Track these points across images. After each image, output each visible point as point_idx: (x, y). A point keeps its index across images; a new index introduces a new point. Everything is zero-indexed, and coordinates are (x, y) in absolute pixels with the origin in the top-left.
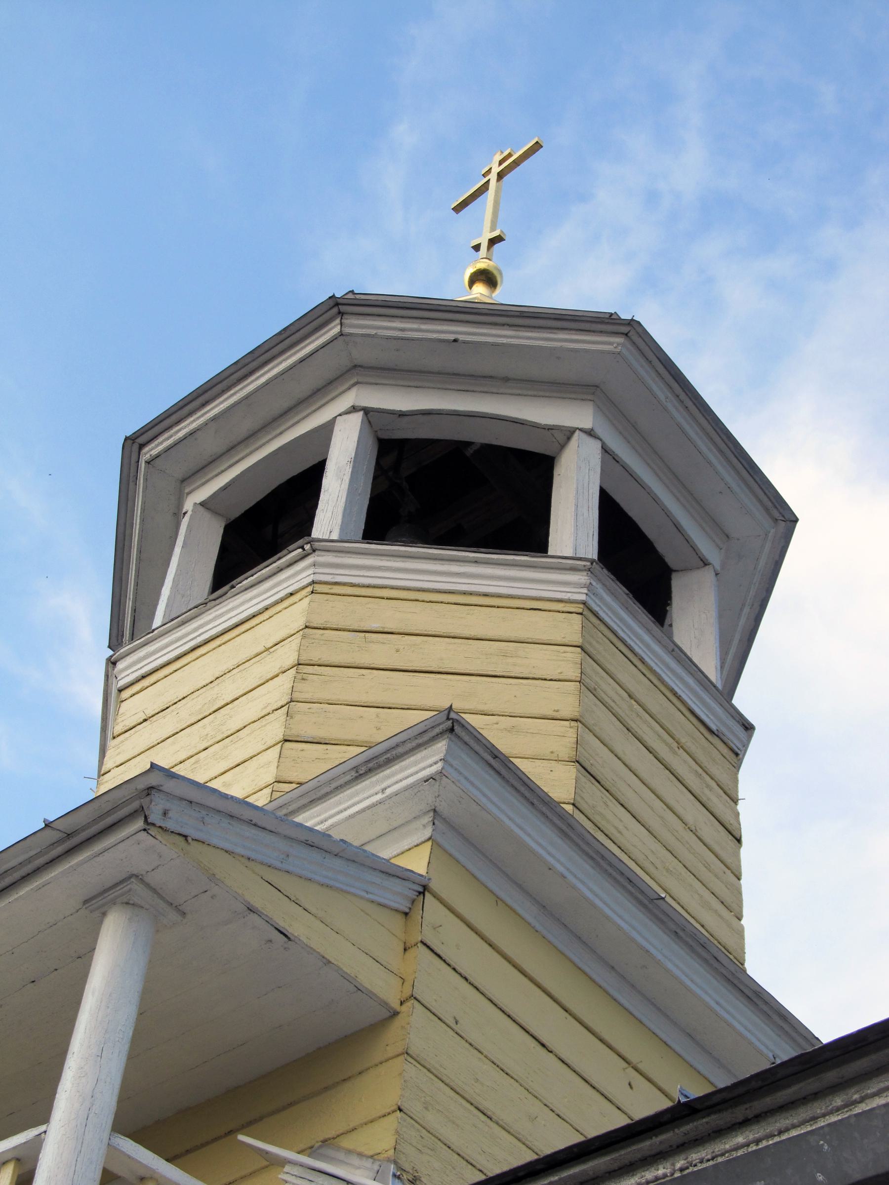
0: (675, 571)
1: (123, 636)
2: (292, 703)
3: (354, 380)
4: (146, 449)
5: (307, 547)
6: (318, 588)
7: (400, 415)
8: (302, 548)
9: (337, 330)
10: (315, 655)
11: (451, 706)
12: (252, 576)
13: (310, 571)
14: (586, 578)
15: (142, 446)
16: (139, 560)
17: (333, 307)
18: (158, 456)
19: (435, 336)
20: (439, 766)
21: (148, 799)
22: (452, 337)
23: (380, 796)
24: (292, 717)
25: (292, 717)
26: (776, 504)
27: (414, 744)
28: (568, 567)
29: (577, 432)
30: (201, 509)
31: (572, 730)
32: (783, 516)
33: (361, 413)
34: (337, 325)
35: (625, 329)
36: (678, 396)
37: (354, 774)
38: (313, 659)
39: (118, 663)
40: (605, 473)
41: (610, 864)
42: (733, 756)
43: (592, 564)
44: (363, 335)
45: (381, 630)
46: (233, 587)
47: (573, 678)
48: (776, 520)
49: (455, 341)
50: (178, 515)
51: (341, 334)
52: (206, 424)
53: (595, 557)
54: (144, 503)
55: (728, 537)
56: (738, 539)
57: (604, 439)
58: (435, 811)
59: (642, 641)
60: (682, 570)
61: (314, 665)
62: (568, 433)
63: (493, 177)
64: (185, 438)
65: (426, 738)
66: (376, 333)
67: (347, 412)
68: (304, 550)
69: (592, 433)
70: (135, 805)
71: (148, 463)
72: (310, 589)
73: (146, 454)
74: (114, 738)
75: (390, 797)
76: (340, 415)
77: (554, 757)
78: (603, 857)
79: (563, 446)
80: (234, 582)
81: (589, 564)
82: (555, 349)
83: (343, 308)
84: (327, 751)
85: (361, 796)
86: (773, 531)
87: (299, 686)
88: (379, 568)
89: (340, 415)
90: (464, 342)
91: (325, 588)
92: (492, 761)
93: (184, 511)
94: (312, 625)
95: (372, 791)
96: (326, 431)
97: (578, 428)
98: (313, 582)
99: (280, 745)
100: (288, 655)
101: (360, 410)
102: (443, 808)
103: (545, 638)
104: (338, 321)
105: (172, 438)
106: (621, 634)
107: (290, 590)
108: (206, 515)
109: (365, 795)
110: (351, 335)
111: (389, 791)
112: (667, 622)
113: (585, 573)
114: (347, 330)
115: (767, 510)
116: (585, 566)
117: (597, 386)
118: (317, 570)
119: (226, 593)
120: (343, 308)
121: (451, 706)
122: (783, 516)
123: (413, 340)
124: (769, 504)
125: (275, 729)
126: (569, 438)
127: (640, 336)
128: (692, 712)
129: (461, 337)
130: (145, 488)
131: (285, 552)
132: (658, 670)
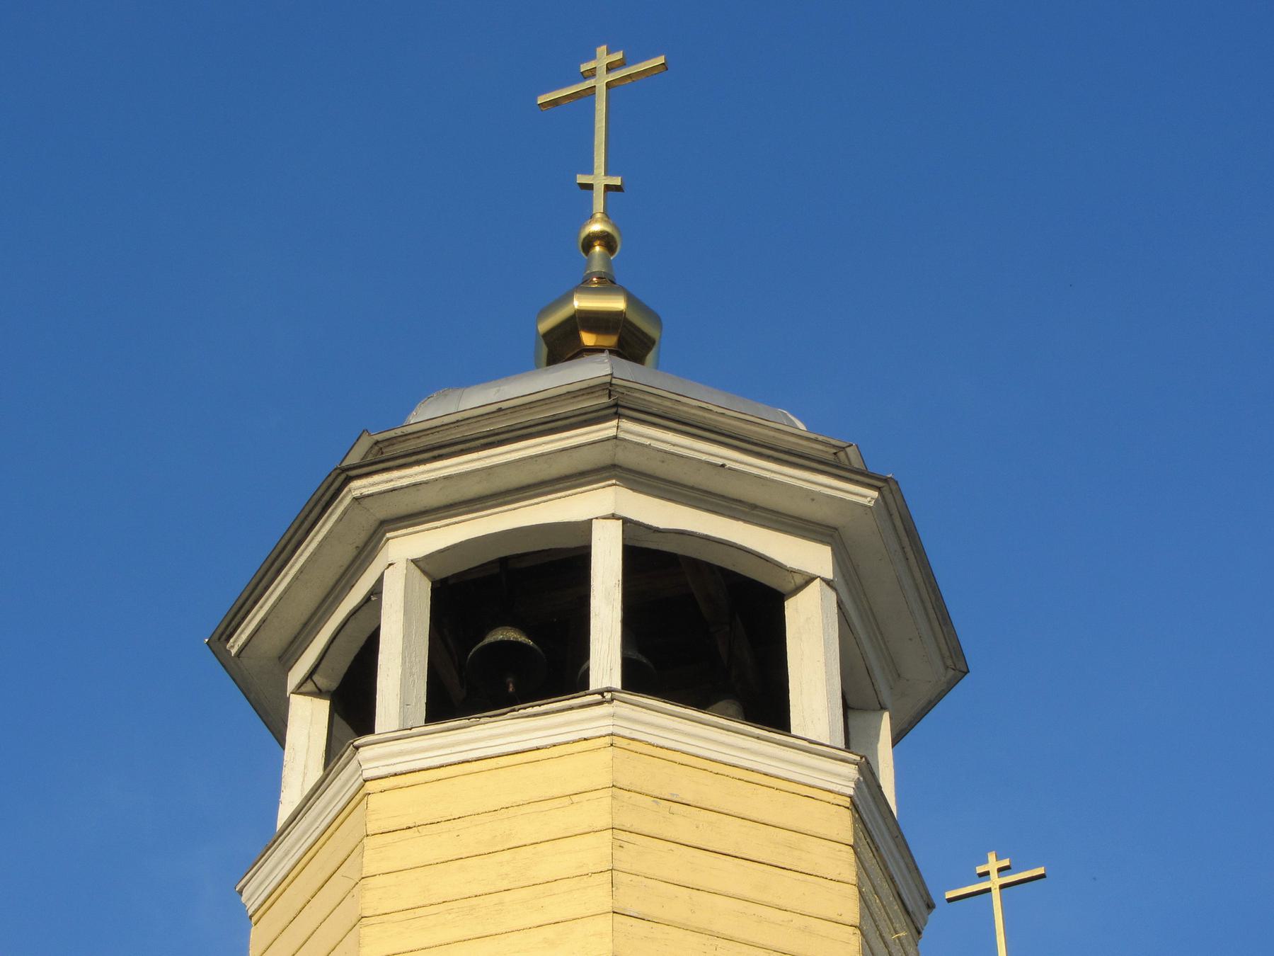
0: (853, 709)
3: (614, 481)
4: (356, 484)
6: (617, 740)
7: (655, 531)
9: (612, 432)
10: (627, 821)
12: (540, 705)
13: (610, 722)
19: (704, 457)
22: (720, 462)
26: (953, 654)
28: (840, 758)
32: (955, 666)
34: (614, 427)
35: (880, 484)
36: (903, 548)
38: (626, 824)
39: (361, 749)
43: (861, 758)
46: (514, 710)
48: (948, 667)
49: (723, 466)
51: (615, 437)
52: (436, 480)
54: (330, 531)
55: (899, 676)
56: (908, 680)
60: (857, 709)
61: (625, 831)
62: (807, 578)
66: (650, 445)
68: (603, 697)
69: (831, 583)
71: (356, 499)
72: (608, 740)
76: (597, 518)
80: (516, 707)
82: (813, 492)
83: (621, 411)
84: (653, 930)
87: (618, 854)
88: (673, 730)
89: (597, 518)
90: (730, 469)
91: (624, 743)
94: (618, 785)
97: (819, 577)
98: (612, 734)
101: (618, 519)
104: (614, 422)
105: (392, 483)
110: (624, 440)
113: (854, 766)
114: (622, 435)
115: (943, 658)
116: (855, 760)
117: (836, 529)
118: (616, 723)
120: (621, 411)
122: (955, 666)
123: (682, 456)
127: (892, 492)
129: (729, 464)
130: (340, 520)
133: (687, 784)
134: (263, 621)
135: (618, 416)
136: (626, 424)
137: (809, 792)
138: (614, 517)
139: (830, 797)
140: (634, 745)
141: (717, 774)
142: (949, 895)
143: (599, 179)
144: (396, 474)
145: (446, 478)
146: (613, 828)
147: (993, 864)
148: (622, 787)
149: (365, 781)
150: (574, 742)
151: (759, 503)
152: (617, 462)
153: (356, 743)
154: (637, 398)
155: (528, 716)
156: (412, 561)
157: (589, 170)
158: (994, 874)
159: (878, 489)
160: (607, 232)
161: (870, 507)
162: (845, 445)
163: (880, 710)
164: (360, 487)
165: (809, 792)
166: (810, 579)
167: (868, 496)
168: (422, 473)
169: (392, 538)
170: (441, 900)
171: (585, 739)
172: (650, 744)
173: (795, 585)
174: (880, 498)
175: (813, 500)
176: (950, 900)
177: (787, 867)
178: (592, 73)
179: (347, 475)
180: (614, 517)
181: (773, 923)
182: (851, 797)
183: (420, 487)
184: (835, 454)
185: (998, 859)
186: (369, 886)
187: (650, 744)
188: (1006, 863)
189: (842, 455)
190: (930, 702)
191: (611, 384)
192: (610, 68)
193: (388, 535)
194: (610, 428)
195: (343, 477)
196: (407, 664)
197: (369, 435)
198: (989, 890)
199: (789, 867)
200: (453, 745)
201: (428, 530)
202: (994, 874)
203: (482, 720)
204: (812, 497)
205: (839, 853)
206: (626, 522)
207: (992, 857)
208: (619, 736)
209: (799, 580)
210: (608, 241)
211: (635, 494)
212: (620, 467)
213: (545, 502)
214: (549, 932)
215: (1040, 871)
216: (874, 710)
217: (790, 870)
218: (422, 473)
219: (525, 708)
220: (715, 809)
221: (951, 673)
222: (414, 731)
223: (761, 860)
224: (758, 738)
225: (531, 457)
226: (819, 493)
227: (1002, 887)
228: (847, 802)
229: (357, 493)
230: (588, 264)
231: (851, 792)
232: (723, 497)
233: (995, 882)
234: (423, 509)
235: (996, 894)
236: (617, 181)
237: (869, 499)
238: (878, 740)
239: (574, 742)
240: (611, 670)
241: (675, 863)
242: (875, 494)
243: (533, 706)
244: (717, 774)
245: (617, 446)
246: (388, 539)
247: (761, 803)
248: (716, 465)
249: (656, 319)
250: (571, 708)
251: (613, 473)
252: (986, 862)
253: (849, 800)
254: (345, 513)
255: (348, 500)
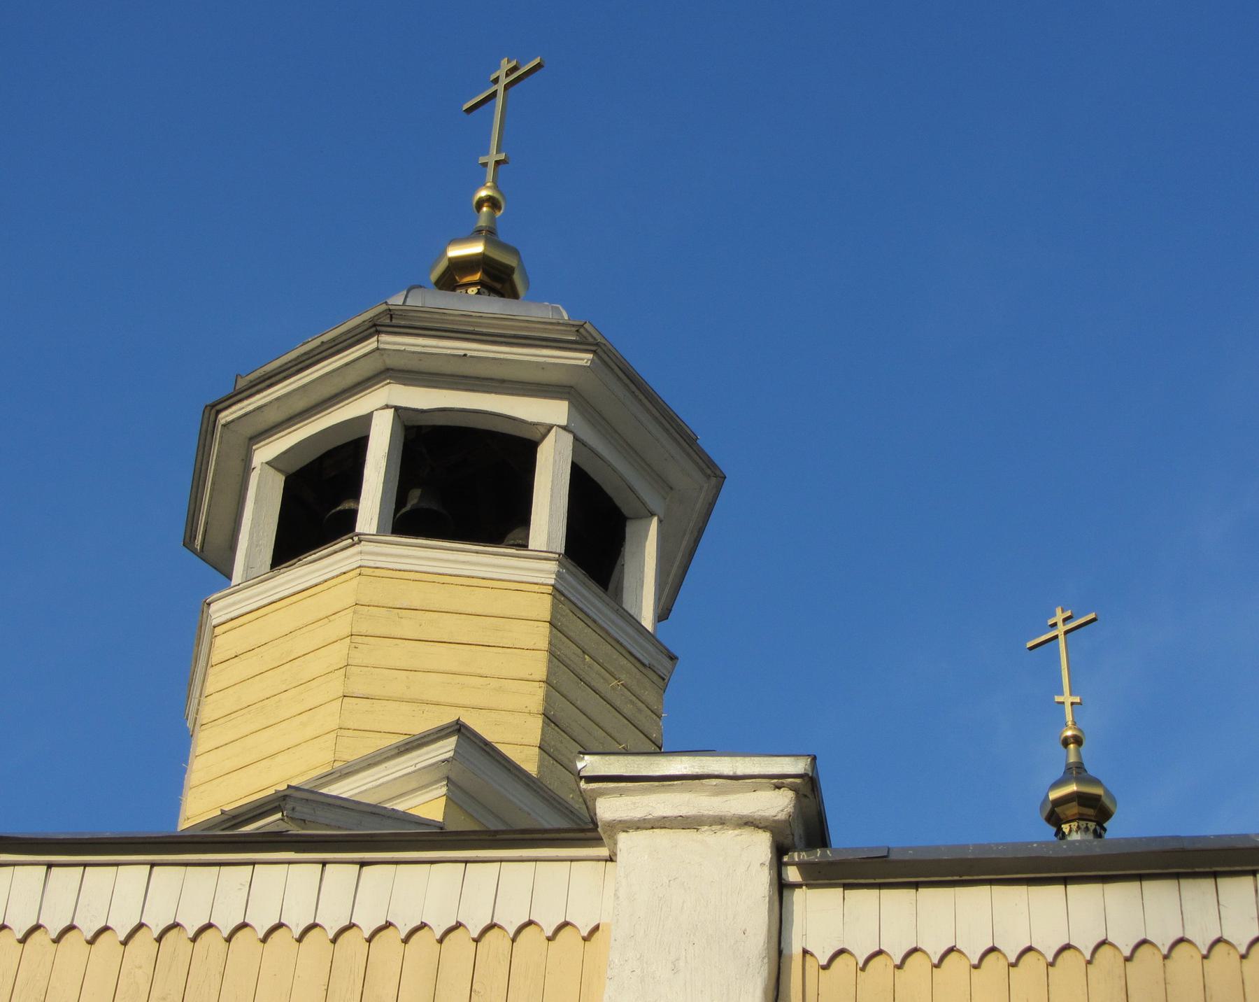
1: (195, 538)
2: (348, 667)
3: (388, 381)
4: (222, 415)
5: (356, 539)
6: (364, 571)
8: (352, 538)
9: (374, 345)
11: (459, 719)
12: (315, 554)
14: (555, 566)
15: (219, 412)
16: (212, 490)
17: (371, 327)
18: (233, 421)
19: (449, 352)
20: (451, 754)
21: (284, 802)
22: (462, 353)
23: (413, 769)
24: (348, 678)
25: (348, 678)
27: (435, 737)
29: (555, 427)
30: (267, 466)
31: (540, 690)
33: (393, 410)
35: (593, 348)
37: (397, 751)
39: (211, 605)
40: (575, 452)
41: (559, 803)
42: (661, 680)
44: (394, 350)
45: (409, 607)
46: (300, 560)
47: (543, 648)
49: (465, 355)
50: (247, 468)
51: (378, 349)
52: (271, 402)
53: (563, 552)
54: (219, 451)
57: (575, 431)
58: (448, 778)
59: (595, 606)
63: (500, 87)
64: (254, 410)
65: (443, 733)
66: (405, 350)
67: (382, 408)
68: (353, 540)
70: (277, 804)
71: (224, 426)
72: (358, 571)
73: (222, 419)
74: (212, 666)
75: (420, 769)
76: (376, 410)
77: (527, 710)
78: (554, 799)
79: (544, 436)
80: (301, 557)
81: (557, 556)
83: (379, 328)
85: (401, 767)
86: (706, 486)
89: (376, 410)
90: (471, 357)
91: (369, 571)
92: (485, 747)
93: (253, 467)
94: (360, 603)
95: (409, 764)
96: (366, 420)
98: (360, 567)
99: (341, 698)
100: (342, 626)
101: (391, 408)
102: (453, 776)
103: (524, 615)
104: (375, 338)
105: (244, 410)
106: (580, 604)
107: (344, 570)
108: (271, 471)
109: (405, 766)
110: (385, 349)
111: (419, 766)
112: (611, 586)
114: (381, 346)
115: (702, 470)
117: (572, 387)
119: (295, 564)
120: (379, 328)
121: (459, 719)
122: (715, 474)
124: (704, 466)
125: (336, 686)
126: (549, 431)
128: (631, 653)
129: (469, 353)
131: (339, 540)
132: (605, 626)
133: (415, 595)
134: (206, 523)
135: (378, 333)
136: (384, 338)
137: (519, 586)
138: (387, 407)
139: (536, 588)
140: (378, 572)
141: (443, 583)
142: (1029, 645)
143: (493, 156)
144: (246, 403)
145: (278, 399)
146: (352, 635)
147: (1059, 616)
148: (363, 604)
149: (214, 627)
150: (451, 575)
151: (506, 378)
152: (388, 367)
153: (207, 601)
154: (412, 316)
155: (310, 563)
156: (267, 463)
157: (1061, 693)
158: (1060, 624)
159: (594, 352)
160: (489, 196)
161: (589, 367)
162: (582, 323)
163: (650, 517)
164: (226, 416)
165: (519, 586)
166: (550, 428)
167: (585, 358)
168: (261, 399)
169: (257, 449)
170: (246, 705)
171: (344, 573)
172: (390, 569)
173: (541, 434)
174: (595, 358)
175: (543, 369)
176: (1031, 648)
177: (490, 644)
178: (496, 81)
179: (216, 408)
180: (387, 407)
181: (473, 687)
182: (553, 586)
183: (262, 409)
184: (577, 331)
185: (1063, 611)
186: (208, 702)
187: (390, 569)
188: (1068, 614)
189: (582, 330)
190: (710, 504)
191: (390, 310)
192: (1065, 620)
193: (254, 447)
194: (373, 342)
195: (213, 411)
196: (254, 538)
197: (242, 378)
198: (1056, 637)
199: (493, 645)
200: (265, 592)
201: (278, 439)
202: (1060, 624)
203: (282, 571)
204: (542, 366)
205: (537, 629)
206: (397, 409)
207: (1059, 611)
208: (365, 567)
209: (543, 430)
210: (493, 202)
211: (407, 387)
212: (392, 369)
213: (347, 404)
214: (304, 717)
215: (1092, 616)
216: (647, 517)
217: (494, 646)
218: (261, 399)
219: (306, 558)
220: (438, 610)
221: (714, 480)
222: (241, 586)
223: (470, 643)
224: (477, 553)
225: (327, 374)
226: (545, 363)
227: (1066, 633)
228: (550, 589)
229: (223, 422)
230: (477, 218)
231: (552, 582)
232: (477, 378)
233: (1061, 628)
234: (273, 425)
235: (1062, 638)
236: (1077, 700)
237: (585, 361)
238: (647, 539)
239: (451, 575)
240: (371, 519)
241: (398, 654)
242: (590, 356)
243: (311, 555)
244: (443, 583)
245: (382, 355)
246: (255, 450)
247: (477, 600)
248: (459, 356)
249: (514, 251)
250: (336, 552)
251: (388, 375)
252: (1054, 615)
253: (551, 588)
254: (221, 437)
255: (220, 426)
